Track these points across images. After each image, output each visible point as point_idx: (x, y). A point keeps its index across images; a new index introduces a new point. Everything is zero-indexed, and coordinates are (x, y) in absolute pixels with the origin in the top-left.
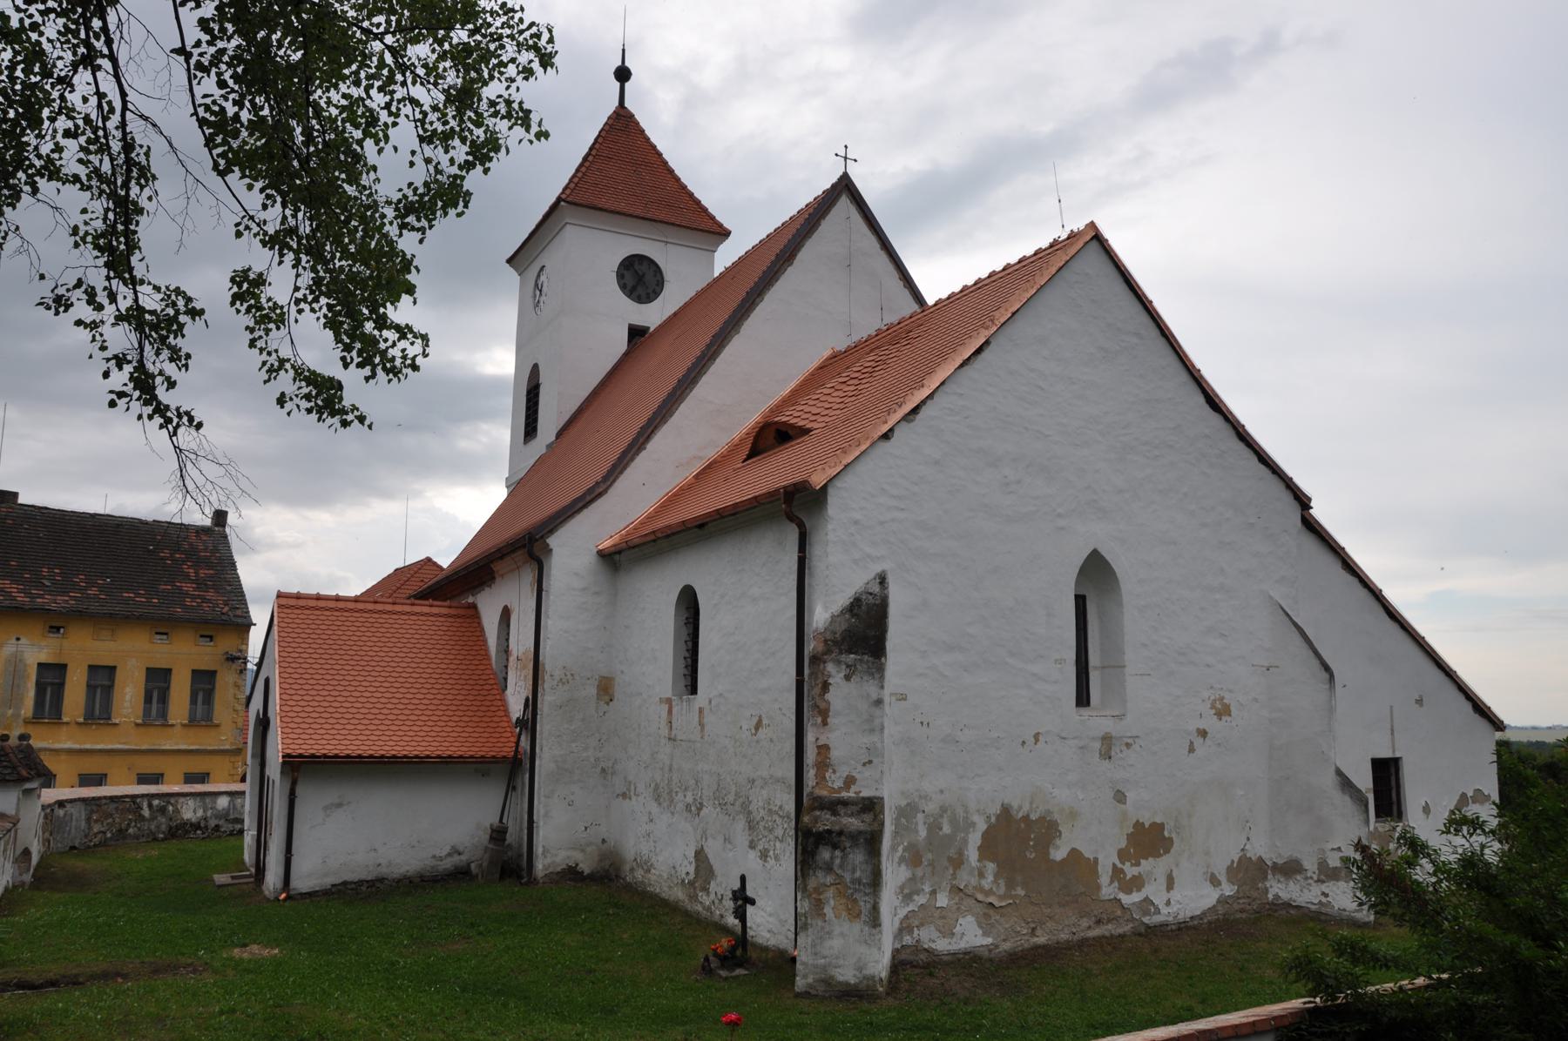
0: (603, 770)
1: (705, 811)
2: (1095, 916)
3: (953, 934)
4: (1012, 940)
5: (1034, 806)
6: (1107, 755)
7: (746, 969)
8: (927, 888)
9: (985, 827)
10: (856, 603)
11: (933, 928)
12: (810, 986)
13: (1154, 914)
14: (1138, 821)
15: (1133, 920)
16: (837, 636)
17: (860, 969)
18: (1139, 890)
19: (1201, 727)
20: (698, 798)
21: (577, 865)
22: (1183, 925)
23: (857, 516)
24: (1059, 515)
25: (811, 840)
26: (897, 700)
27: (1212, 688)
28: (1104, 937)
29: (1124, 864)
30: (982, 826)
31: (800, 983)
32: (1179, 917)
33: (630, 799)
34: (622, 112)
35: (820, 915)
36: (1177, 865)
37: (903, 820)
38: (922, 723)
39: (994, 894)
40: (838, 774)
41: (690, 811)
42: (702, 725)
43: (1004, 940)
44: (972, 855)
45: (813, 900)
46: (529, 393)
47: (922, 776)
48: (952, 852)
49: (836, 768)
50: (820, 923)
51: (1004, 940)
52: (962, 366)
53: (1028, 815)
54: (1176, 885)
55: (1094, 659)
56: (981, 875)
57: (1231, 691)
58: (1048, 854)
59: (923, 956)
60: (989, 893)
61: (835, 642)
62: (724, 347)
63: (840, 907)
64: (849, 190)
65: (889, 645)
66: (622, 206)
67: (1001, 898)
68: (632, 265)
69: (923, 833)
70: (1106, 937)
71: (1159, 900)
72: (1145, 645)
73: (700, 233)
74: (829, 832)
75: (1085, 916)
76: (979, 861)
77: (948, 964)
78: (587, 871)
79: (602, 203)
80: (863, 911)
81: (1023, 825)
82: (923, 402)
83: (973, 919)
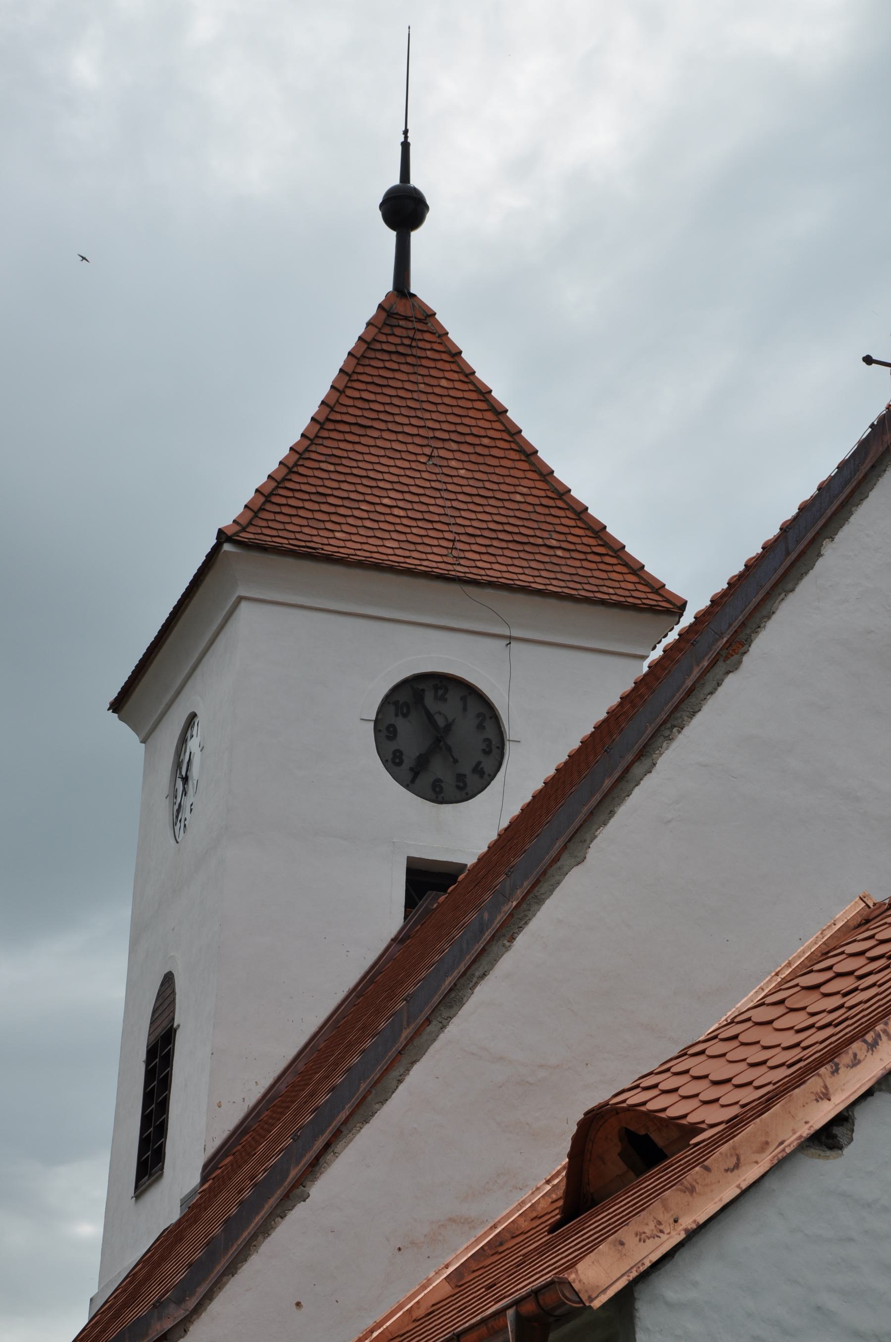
34: (401, 308)
46: (151, 1053)
62: (540, 902)
68: (419, 697)
73: (553, 602)
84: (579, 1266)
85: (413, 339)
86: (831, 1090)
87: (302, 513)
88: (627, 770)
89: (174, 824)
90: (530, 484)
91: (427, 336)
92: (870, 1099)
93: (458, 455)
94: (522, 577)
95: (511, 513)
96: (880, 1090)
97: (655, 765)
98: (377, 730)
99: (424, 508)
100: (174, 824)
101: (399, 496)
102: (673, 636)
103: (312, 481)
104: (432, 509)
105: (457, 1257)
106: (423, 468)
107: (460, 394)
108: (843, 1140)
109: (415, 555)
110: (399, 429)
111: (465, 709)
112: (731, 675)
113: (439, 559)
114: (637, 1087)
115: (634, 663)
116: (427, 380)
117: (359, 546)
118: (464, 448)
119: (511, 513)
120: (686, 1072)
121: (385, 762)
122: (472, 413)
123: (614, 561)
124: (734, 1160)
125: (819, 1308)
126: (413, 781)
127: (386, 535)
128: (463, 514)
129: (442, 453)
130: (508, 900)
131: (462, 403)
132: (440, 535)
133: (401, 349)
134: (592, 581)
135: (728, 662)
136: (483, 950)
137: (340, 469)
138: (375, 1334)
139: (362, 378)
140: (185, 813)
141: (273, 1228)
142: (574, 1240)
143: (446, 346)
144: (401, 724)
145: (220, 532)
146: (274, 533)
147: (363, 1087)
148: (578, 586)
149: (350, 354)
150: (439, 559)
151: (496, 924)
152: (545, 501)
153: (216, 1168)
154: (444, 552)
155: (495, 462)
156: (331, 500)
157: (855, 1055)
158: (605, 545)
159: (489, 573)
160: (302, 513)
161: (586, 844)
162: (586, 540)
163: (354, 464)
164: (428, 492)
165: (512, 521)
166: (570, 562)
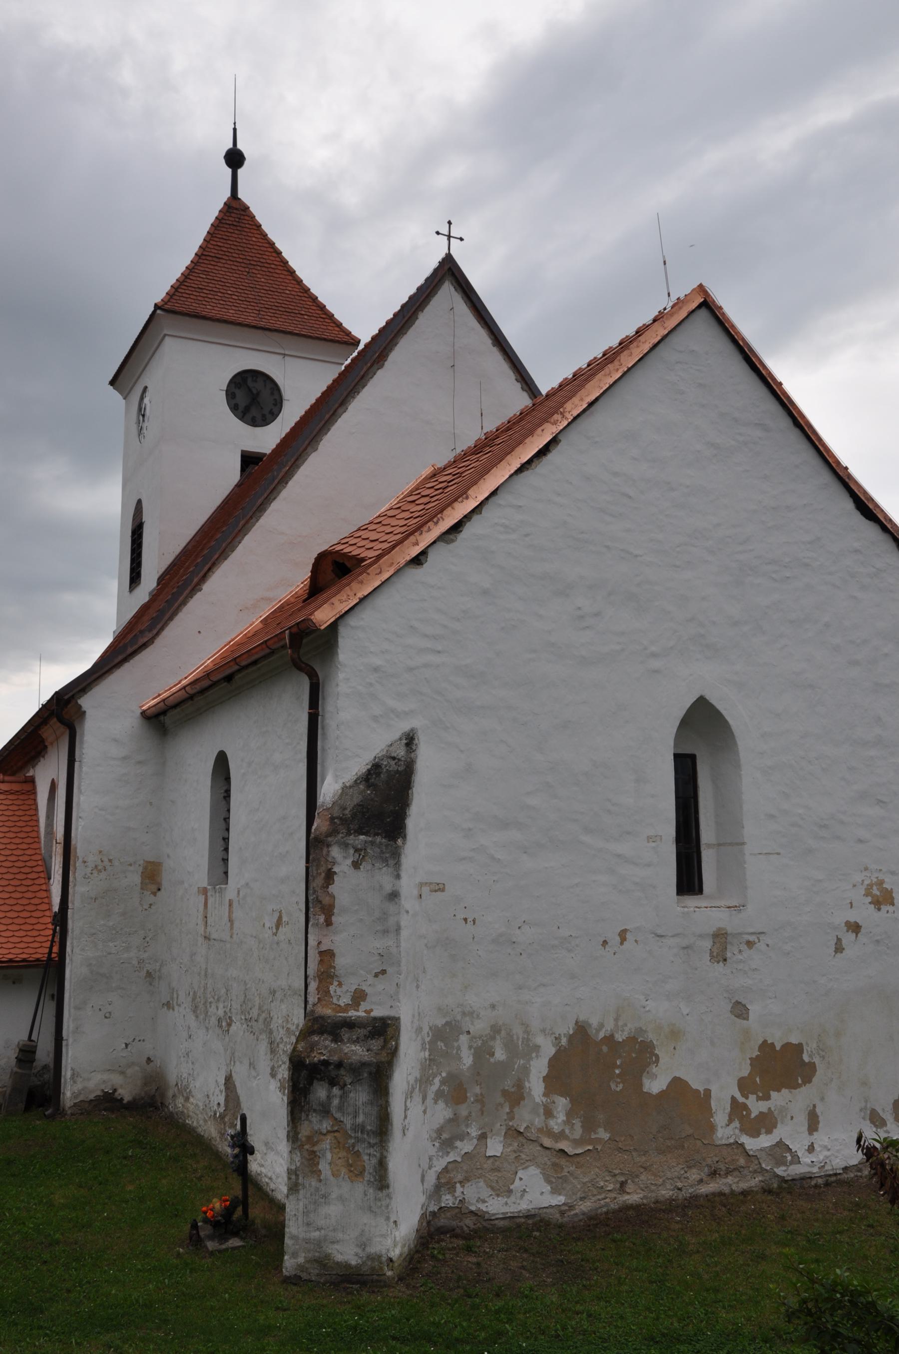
0: (149, 974)
1: (234, 1028)
2: (709, 1166)
3: (510, 1191)
4: (594, 1199)
5: (620, 1023)
6: (720, 956)
7: (242, 1239)
8: (474, 1132)
9: (552, 1051)
10: (376, 768)
11: (482, 1184)
12: (301, 1267)
13: (792, 1163)
14: (765, 1041)
15: (763, 1171)
16: (347, 812)
17: (363, 1246)
18: (769, 1132)
19: (852, 920)
20: (228, 1010)
21: (115, 1090)
22: (833, 1179)
23: (377, 661)
24: (654, 655)
25: (304, 1073)
26: (431, 891)
27: (866, 869)
28: (721, 1194)
29: (747, 1098)
30: (548, 1050)
31: (289, 1264)
32: (828, 1167)
33: (173, 1010)
34: (234, 204)
35: (313, 1172)
36: (822, 1099)
37: (441, 1044)
38: (466, 920)
39: (566, 1138)
40: (344, 988)
41: (221, 1027)
42: (231, 921)
43: (582, 1199)
44: (536, 1087)
45: (305, 1154)
47: (466, 987)
48: (508, 1084)
49: (342, 980)
50: (314, 1183)
51: (582, 1199)
52: (520, 470)
53: (612, 1036)
54: (821, 1125)
55: (707, 833)
56: (549, 1113)
57: (893, 873)
58: (641, 1085)
59: (469, 1222)
60: (561, 1136)
61: (344, 820)
62: (298, 467)
63: (339, 1162)
64: (453, 275)
65: (412, 823)
66: (231, 314)
67: (576, 1143)
68: (245, 380)
69: (467, 1059)
70: (724, 1195)
71: (798, 1145)
72: (771, 817)
73: (322, 342)
74: (326, 1063)
75: (694, 1166)
76: (545, 1095)
77: (504, 1230)
78: (127, 1098)
79: (207, 310)
80: (367, 1167)
81: (605, 1049)
82: (467, 517)
83: (538, 1171)
84: (316, 613)
85: (240, 219)
86: (419, 541)
87: (192, 297)
88: (335, 411)
89: (139, 435)
90: (293, 286)
91: (246, 218)
92: (435, 545)
93: (261, 272)
94: (289, 327)
95: (284, 299)
96: (439, 541)
97: (347, 409)
98: (227, 395)
99: (246, 296)
100: (139, 435)
101: (235, 290)
102: (355, 354)
103: (196, 282)
104: (250, 296)
105: (265, 613)
106: (245, 277)
107: (261, 244)
108: (423, 562)
109: (242, 316)
110: (234, 259)
111: (265, 386)
112: (380, 370)
113: (253, 318)
114: (339, 543)
115: (339, 366)
116: (246, 238)
117: (217, 312)
118: (263, 269)
119: (284, 299)
120: (360, 537)
121: (231, 409)
122: (267, 253)
123: (329, 321)
124: (379, 570)
125: (411, 627)
126: (243, 417)
127: (229, 308)
128: (264, 299)
129: (254, 271)
130: (285, 466)
131: (262, 249)
132: (253, 308)
133: (235, 223)
134: (320, 330)
135: (379, 364)
136: (274, 488)
137: (208, 277)
138: (232, 643)
139: (217, 236)
140: (144, 431)
141: (188, 602)
142: (312, 605)
143: (254, 222)
144: (238, 392)
145: (156, 305)
146: (180, 305)
147: (224, 545)
148: (314, 332)
149: (212, 225)
150: (253, 318)
151: (280, 477)
152: (299, 294)
153: (163, 579)
154: (255, 315)
155: (277, 276)
156: (205, 291)
157: (429, 527)
158: (325, 314)
159: (275, 325)
160: (192, 297)
161: (318, 443)
162: (317, 312)
163: (214, 275)
164: (248, 289)
165: (285, 302)
166: (311, 321)
